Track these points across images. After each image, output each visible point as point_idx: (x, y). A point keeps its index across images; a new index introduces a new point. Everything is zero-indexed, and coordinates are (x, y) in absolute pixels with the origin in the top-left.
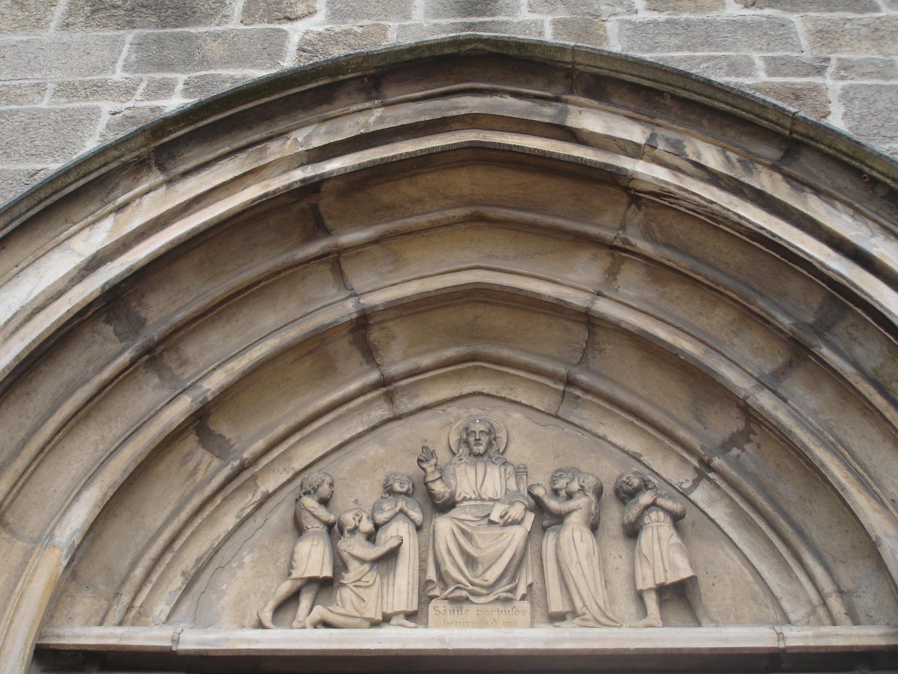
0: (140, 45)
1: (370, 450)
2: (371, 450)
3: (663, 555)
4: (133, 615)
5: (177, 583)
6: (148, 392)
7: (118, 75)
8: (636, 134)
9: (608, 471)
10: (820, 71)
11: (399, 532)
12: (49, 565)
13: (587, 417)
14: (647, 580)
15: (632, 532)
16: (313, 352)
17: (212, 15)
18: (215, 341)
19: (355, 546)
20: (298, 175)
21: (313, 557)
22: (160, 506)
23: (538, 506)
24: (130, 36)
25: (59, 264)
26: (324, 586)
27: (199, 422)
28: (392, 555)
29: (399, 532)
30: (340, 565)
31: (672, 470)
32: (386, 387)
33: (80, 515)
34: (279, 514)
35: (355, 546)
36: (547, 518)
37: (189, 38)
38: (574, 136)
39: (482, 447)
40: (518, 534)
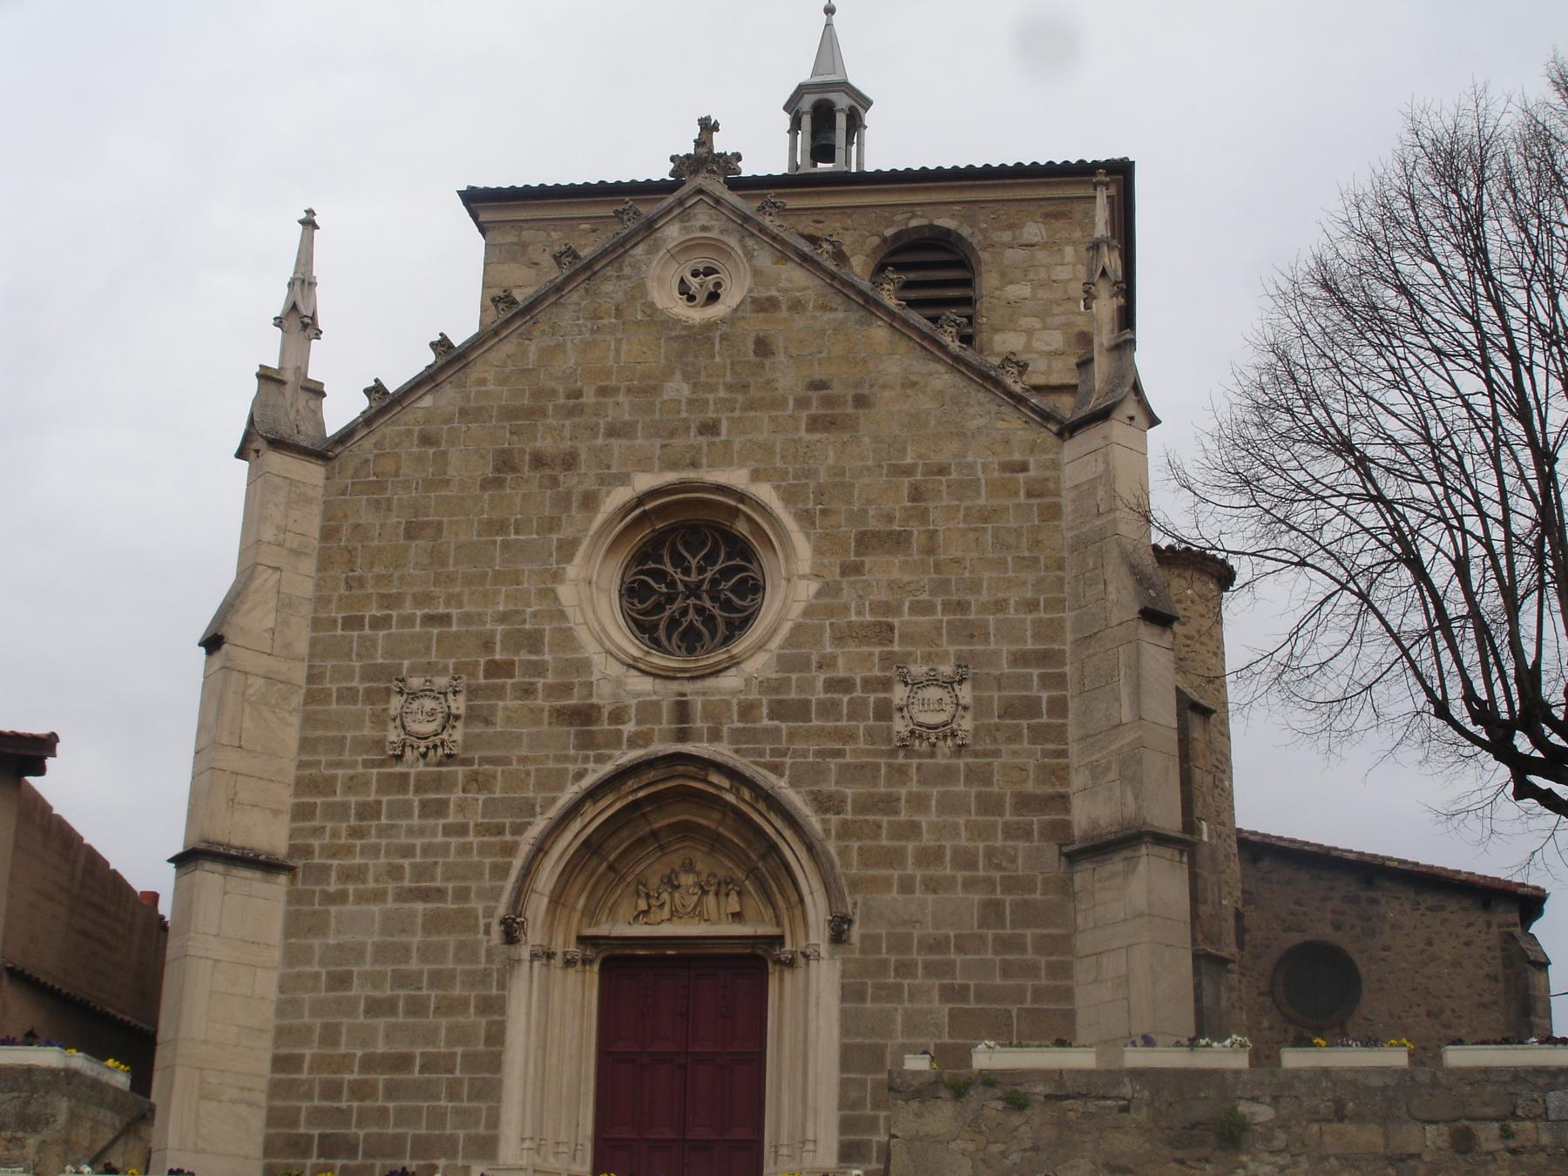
0: (577, 734)
1: (657, 866)
3: (733, 904)
9: (722, 874)
10: (785, 755)
11: (665, 896)
14: (730, 910)
15: (727, 895)
16: (641, 842)
17: (558, 346)
19: (654, 902)
20: (631, 798)
21: (642, 905)
23: (702, 887)
24: (573, 730)
26: (646, 913)
29: (665, 896)
30: (650, 907)
31: (740, 875)
32: (661, 848)
34: (632, 888)
35: (654, 902)
36: (705, 892)
37: (590, 732)
39: (689, 867)
40: (696, 898)
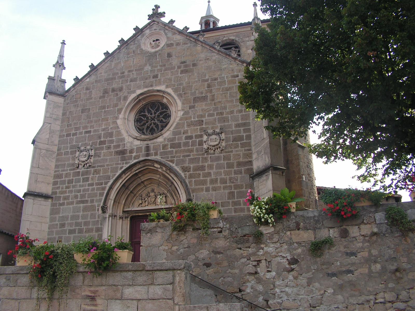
2: (145, 191)
4: (129, 207)
5: (132, 204)
6: (127, 191)
7: (120, 162)
8: (159, 167)
10: (174, 158)
11: (146, 199)
12: (122, 205)
13: (160, 187)
18: (131, 185)
20: (134, 173)
22: (130, 199)
24: (120, 156)
25: (118, 184)
26: (141, 204)
27: (131, 192)
28: (146, 201)
32: (145, 186)
33: (124, 202)
38: (155, 167)
